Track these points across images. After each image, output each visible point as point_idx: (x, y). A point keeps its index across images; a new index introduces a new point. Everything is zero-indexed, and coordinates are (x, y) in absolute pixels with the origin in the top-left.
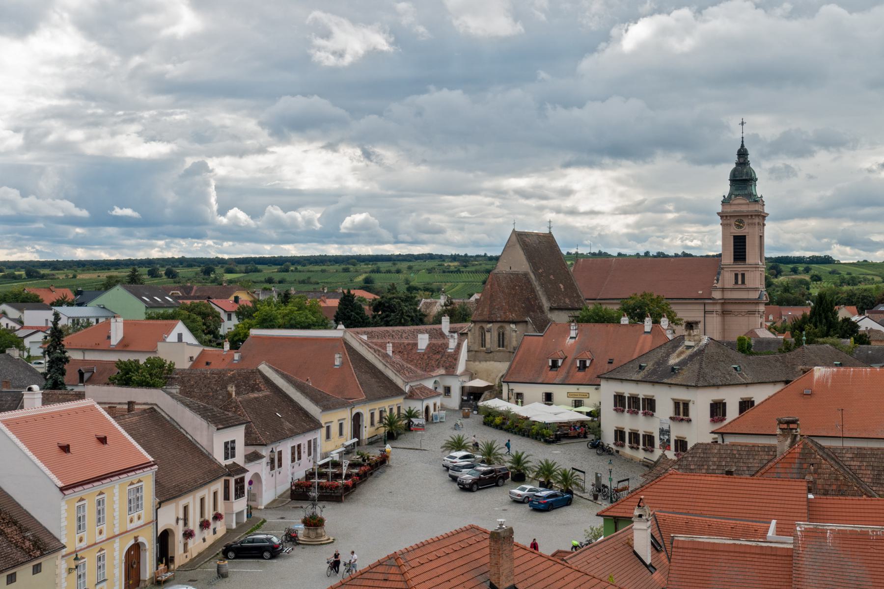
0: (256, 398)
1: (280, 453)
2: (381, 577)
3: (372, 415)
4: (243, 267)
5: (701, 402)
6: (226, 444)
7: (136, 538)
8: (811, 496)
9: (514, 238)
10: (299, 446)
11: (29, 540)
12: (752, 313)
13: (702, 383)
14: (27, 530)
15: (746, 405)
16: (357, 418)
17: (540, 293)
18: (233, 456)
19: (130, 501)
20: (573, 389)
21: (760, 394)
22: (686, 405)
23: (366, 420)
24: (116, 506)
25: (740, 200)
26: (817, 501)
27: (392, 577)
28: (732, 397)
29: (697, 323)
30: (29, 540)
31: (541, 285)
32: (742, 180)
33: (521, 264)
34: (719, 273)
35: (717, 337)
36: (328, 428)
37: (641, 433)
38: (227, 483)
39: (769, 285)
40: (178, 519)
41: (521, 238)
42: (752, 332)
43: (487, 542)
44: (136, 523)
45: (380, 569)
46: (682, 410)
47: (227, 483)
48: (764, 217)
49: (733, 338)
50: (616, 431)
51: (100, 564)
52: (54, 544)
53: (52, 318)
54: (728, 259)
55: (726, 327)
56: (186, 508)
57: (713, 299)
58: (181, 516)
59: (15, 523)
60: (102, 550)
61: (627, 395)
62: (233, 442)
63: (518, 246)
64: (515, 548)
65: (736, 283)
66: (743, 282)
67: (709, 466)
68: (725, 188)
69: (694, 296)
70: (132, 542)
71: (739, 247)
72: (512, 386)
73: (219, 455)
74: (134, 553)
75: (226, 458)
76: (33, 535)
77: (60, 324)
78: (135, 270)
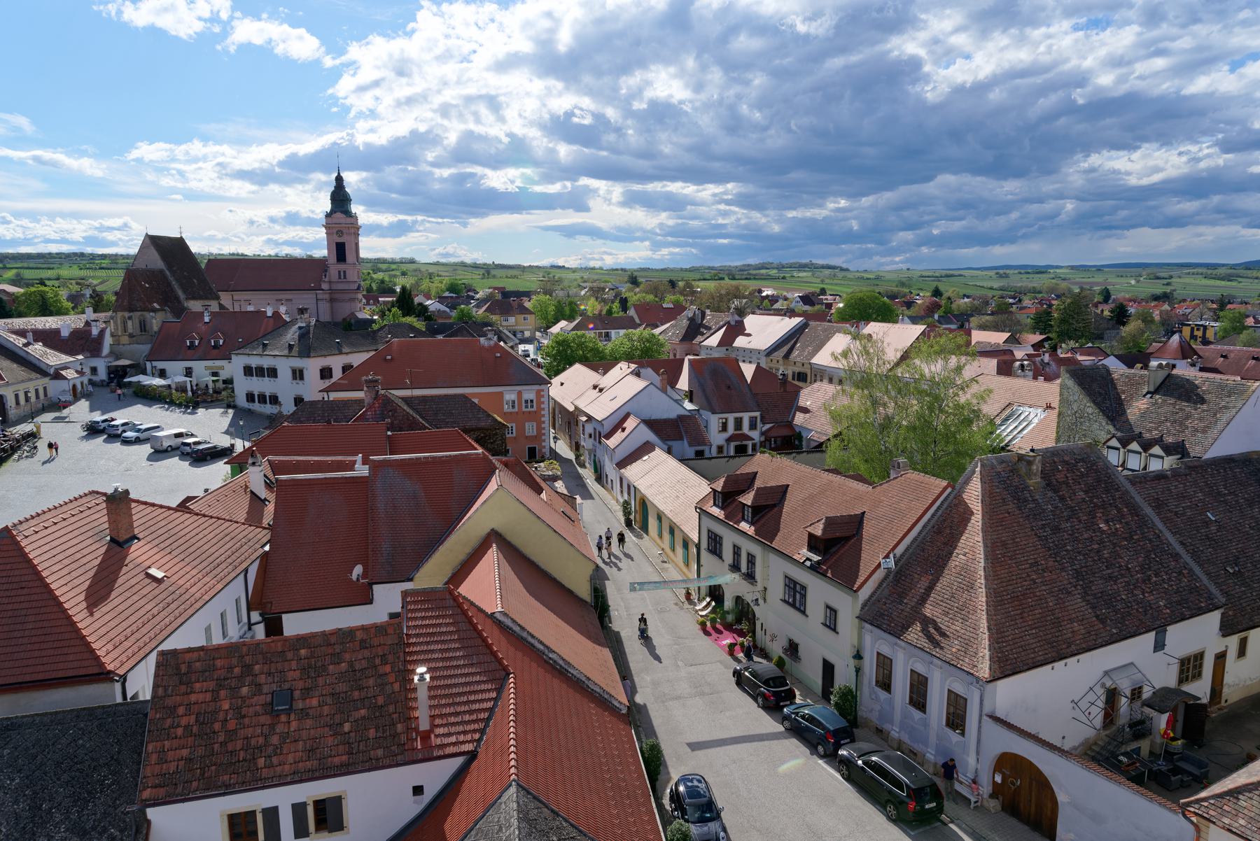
3: (17, 396)
5: (311, 366)
9: (148, 241)
12: (353, 300)
13: (306, 352)
15: (346, 368)
21: (357, 359)
22: (301, 372)
25: (339, 215)
28: (336, 363)
29: (306, 309)
31: (177, 280)
32: (340, 198)
33: (156, 262)
35: (326, 317)
39: (905, 357)
41: (154, 242)
42: (353, 314)
43: (104, 505)
46: (298, 374)
49: (339, 318)
54: (333, 259)
64: (133, 505)
68: (328, 207)
72: (155, 363)
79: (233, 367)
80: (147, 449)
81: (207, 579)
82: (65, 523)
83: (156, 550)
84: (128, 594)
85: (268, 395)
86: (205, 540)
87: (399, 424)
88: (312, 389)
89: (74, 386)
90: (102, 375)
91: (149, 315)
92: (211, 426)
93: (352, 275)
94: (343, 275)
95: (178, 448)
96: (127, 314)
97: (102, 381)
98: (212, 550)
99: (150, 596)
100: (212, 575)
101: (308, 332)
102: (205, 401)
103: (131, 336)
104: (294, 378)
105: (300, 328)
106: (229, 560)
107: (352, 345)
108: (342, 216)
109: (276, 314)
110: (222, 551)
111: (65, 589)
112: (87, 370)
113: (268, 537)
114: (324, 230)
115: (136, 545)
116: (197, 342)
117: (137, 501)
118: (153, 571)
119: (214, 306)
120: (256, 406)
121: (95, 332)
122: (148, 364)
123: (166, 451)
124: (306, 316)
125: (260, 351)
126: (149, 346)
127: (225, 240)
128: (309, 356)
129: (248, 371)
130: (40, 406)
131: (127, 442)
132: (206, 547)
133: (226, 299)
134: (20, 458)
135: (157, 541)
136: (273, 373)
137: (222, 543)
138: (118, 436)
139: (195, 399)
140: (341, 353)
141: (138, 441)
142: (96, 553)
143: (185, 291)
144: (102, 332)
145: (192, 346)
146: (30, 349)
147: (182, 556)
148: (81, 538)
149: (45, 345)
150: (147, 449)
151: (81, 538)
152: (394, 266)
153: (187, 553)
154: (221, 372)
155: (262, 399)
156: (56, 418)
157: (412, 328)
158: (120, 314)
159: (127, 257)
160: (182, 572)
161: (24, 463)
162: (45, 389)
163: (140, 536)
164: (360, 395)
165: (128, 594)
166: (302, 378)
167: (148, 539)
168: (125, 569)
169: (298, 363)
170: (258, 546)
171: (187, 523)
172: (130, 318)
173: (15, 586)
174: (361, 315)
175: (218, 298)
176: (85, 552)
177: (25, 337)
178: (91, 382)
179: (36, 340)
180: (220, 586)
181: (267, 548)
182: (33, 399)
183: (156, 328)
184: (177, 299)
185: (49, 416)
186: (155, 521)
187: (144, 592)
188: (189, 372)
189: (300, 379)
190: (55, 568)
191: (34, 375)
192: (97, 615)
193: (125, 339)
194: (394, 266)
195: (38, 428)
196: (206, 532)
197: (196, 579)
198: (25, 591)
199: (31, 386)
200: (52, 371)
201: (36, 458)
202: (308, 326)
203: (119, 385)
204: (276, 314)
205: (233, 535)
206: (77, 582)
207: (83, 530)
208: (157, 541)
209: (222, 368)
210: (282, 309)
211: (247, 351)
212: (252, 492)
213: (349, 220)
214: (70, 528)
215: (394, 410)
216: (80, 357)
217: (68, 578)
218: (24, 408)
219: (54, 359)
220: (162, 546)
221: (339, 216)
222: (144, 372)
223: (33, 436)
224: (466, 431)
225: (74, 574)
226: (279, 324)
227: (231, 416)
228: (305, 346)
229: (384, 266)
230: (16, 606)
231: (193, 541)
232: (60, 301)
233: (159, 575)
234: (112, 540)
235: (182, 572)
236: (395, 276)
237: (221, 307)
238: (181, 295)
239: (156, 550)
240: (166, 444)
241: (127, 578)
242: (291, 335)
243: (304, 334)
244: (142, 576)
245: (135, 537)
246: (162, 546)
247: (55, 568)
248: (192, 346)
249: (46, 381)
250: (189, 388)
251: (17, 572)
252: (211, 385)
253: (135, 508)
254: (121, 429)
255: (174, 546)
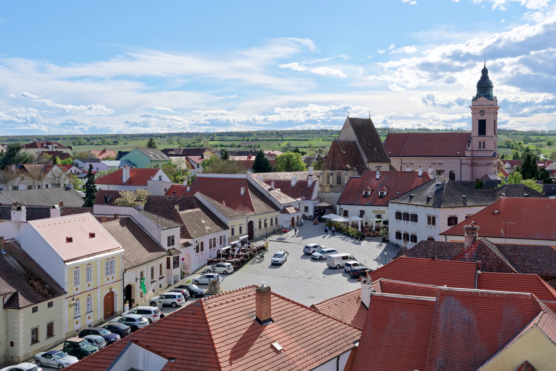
0: (190, 212)
1: (202, 243)
2: (191, 312)
3: (260, 222)
4: (219, 138)
5: (442, 215)
6: (169, 238)
7: (111, 289)
8: (479, 272)
9: (348, 121)
10: (214, 239)
11: (47, 289)
12: (489, 165)
13: (438, 204)
14: (46, 284)
16: (250, 224)
17: (362, 153)
18: (173, 244)
19: (107, 269)
20: (376, 208)
22: (434, 219)
23: (256, 226)
24: (99, 271)
25: (483, 99)
26: (483, 275)
27: (197, 313)
28: (461, 214)
29: (443, 171)
30: (47, 289)
31: (363, 148)
32: (484, 86)
33: (352, 136)
34: (470, 142)
36: (233, 230)
37: (402, 233)
38: (168, 260)
40: (137, 279)
44: (111, 280)
45: (191, 308)
46: (432, 221)
47: (168, 260)
48: (497, 109)
50: (397, 233)
51: (89, 303)
52: (60, 291)
53: (89, 168)
55: (474, 173)
56: (142, 273)
57: (466, 156)
58: (139, 277)
59: (40, 280)
60: (89, 295)
61: (402, 212)
62: (173, 236)
63: (350, 126)
64: (272, 296)
65: (480, 147)
66: (484, 147)
67: (427, 254)
69: (454, 154)
70: (109, 291)
71: (482, 127)
72: (342, 206)
73: (164, 244)
74: (109, 299)
75: (169, 245)
76: (49, 287)
77: (93, 170)
78: (151, 140)
79: (389, 212)
80: (324, 265)
81: (309, 358)
82: (233, 303)
83: (282, 331)
84: (256, 356)
85: (410, 234)
86: (316, 330)
87: (488, 265)
88: (438, 232)
89: (293, 219)
90: (311, 213)
91: (343, 173)
92: (369, 254)
93: (489, 145)
94: (482, 145)
95: (343, 267)
96: (330, 172)
97: (310, 216)
98: (318, 338)
99: (270, 361)
100: (313, 355)
101: (442, 189)
102: (369, 236)
103: (331, 187)
104: (429, 223)
105: (437, 185)
106: (328, 348)
107: (475, 200)
108: (485, 99)
109: (425, 174)
110: (325, 340)
111: (221, 344)
112: (302, 209)
113: (358, 338)
114: (470, 111)
115: (270, 325)
116: (369, 193)
117: (276, 295)
118: (276, 345)
119: (385, 167)
120: (401, 243)
121: (310, 183)
122: (338, 207)
123: (336, 268)
124: (442, 176)
125: (407, 201)
126: (340, 194)
127: (308, 122)
128: (440, 207)
129: (398, 215)
130: (272, 230)
131: (314, 259)
132: (315, 335)
133: (396, 162)
134: (254, 262)
135: (284, 325)
136: (414, 218)
137: (326, 334)
138: (310, 254)
139: (363, 234)
140: (465, 206)
141: (321, 259)
142: (245, 324)
143: (367, 157)
144: (314, 183)
145: (366, 196)
146: (271, 193)
147: (297, 338)
148: (239, 314)
149: (282, 191)
150: (324, 265)
151: (239, 314)
152: (542, 138)
153: (301, 337)
154: (383, 215)
155: (406, 236)
156: (279, 239)
157: (527, 189)
158: (326, 171)
159: (332, 132)
160: (294, 349)
161: (255, 266)
162: (276, 219)
163: (275, 320)
164: (461, 239)
165: (256, 356)
166: (434, 224)
167: (279, 322)
168: (259, 340)
169: (432, 212)
170: (351, 341)
171: (307, 316)
172: (332, 174)
173: (197, 337)
174: (492, 177)
175: (389, 161)
176: (239, 323)
177: (270, 184)
178: (304, 217)
179: (276, 187)
180: (316, 364)
181: (357, 344)
182: (269, 225)
183: (346, 182)
184: (362, 161)
185: (275, 237)
186: (286, 311)
187: (267, 357)
188: (362, 213)
189: (431, 223)
190: (219, 330)
191: (271, 209)
192: (234, 366)
193: (327, 189)
194: (542, 138)
195: (267, 244)
196: (317, 325)
197: (302, 356)
198: (201, 341)
199: (269, 217)
200: (281, 208)
201: (262, 263)
202: (443, 184)
203: (319, 220)
204: (425, 174)
205: (335, 330)
206: (229, 342)
207: (242, 309)
208: (284, 325)
209: (384, 212)
210: (430, 171)
211: (399, 201)
212: (362, 302)
213: (490, 102)
214: (230, 308)
215: (487, 254)
216: (299, 199)
217: (225, 338)
218: (263, 231)
219: (283, 199)
220: (287, 329)
221: (483, 100)
222: (335, 213)
223: (263, 249)
224: (546, 279)
225: (229, 337)
226: (426, 180)
227: (383, 248)
228: (438, 201)
229: (534, 138)
230: (195, 350)
231: (307, 329)
232: (299, 162)
233: (279, 347)
234: (257, 319)
235: (294, 349)
236: (541, 146)
237: (391, 167)
238: (365, 159)
239: (282, 331)
240: (336, 263)
241: (259, 345)
242: (431, 190)
243: (439, 191)
244: (269, 346)
245: (271, 320)
246: (287, 329)
247: (219, 330)
248: (366, 196)
249: (277, 214)
250: (360, 225)
251: (200, 329)
252: (375, 225)
253: (273, 298)
254: (312, 250)
255: (294, 331)
